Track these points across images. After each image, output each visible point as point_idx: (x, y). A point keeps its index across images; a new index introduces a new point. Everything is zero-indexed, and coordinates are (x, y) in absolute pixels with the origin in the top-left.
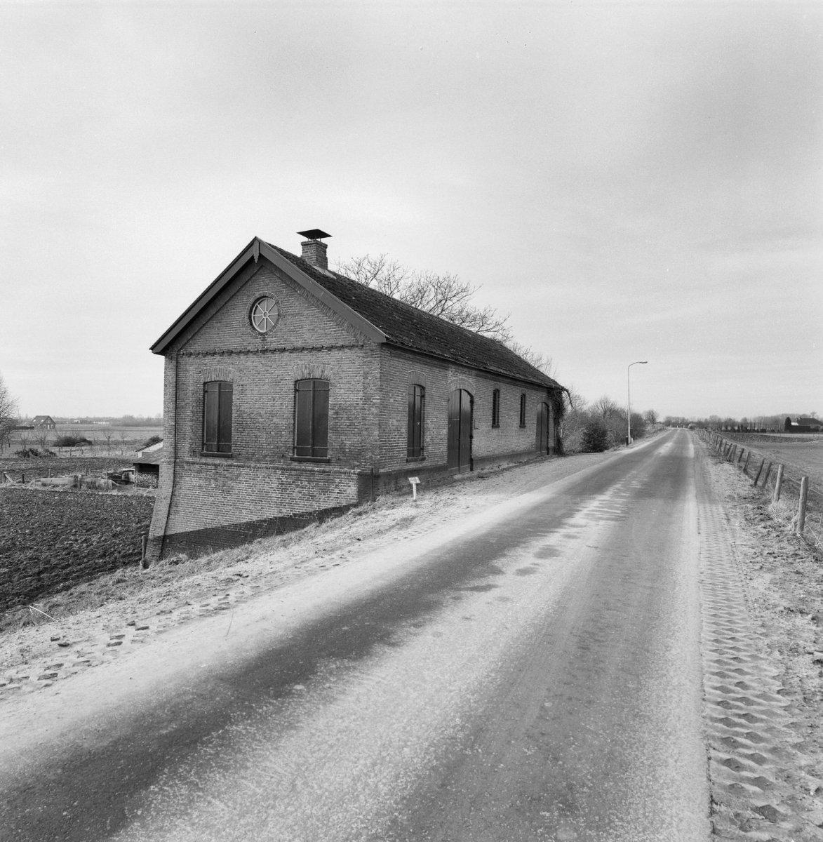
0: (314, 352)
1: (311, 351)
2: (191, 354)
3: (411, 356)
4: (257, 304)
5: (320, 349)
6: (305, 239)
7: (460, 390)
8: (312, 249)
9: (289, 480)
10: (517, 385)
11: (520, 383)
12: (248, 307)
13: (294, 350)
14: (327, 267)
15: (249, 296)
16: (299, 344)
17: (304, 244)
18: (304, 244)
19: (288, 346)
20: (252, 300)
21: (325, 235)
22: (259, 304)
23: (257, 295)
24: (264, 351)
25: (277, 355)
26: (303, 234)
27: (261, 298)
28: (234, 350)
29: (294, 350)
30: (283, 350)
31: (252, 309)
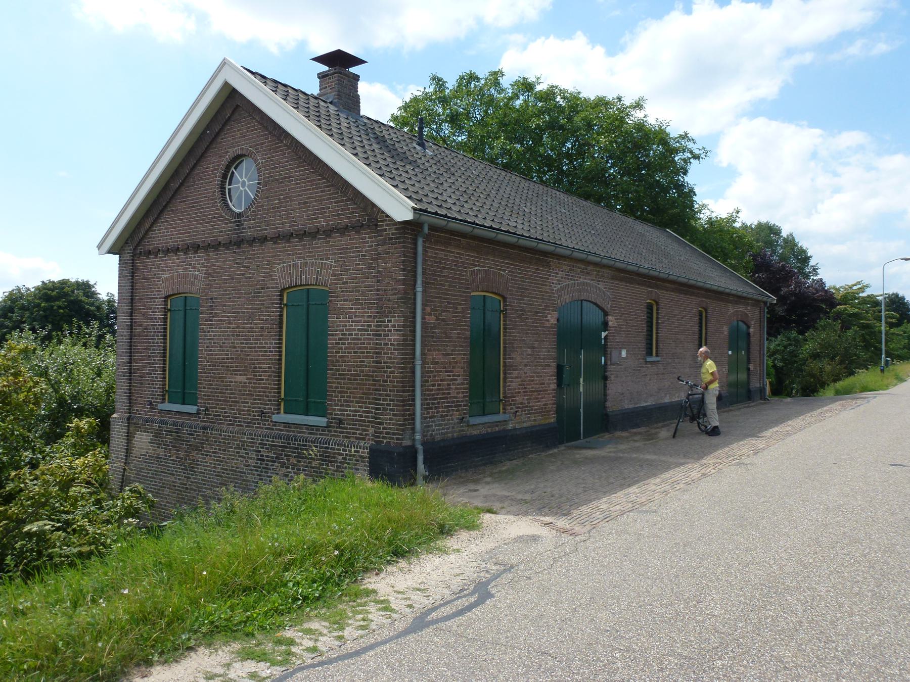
0: (306, 241)
1: (301, 240)
2: (149, 253)
3: (630, 268)
4: (233, 169)
5: (314, 234)
6: (324, 68)
7: (582, 300)
8: (333, 81)
9: (271, 455)
10: (692, 294)
11: (696, 291)
12: (221, 171)
13: (277, 238)
14: (359, 110)
15: (221, 156)
16: (287, 227)
17: (322, 76)
18: (322, 76)
19: (269, 232)
20: (225, 161)
21: (358, 61)
22: (236, 168)
23: (232, 153)
24: (239, 243)
25: (256, 248)
26: (320, 59)
27: (236, 160)
28: (201, 244)
29: (277, 238)
30: (264, 240)
31: (227, 176)
